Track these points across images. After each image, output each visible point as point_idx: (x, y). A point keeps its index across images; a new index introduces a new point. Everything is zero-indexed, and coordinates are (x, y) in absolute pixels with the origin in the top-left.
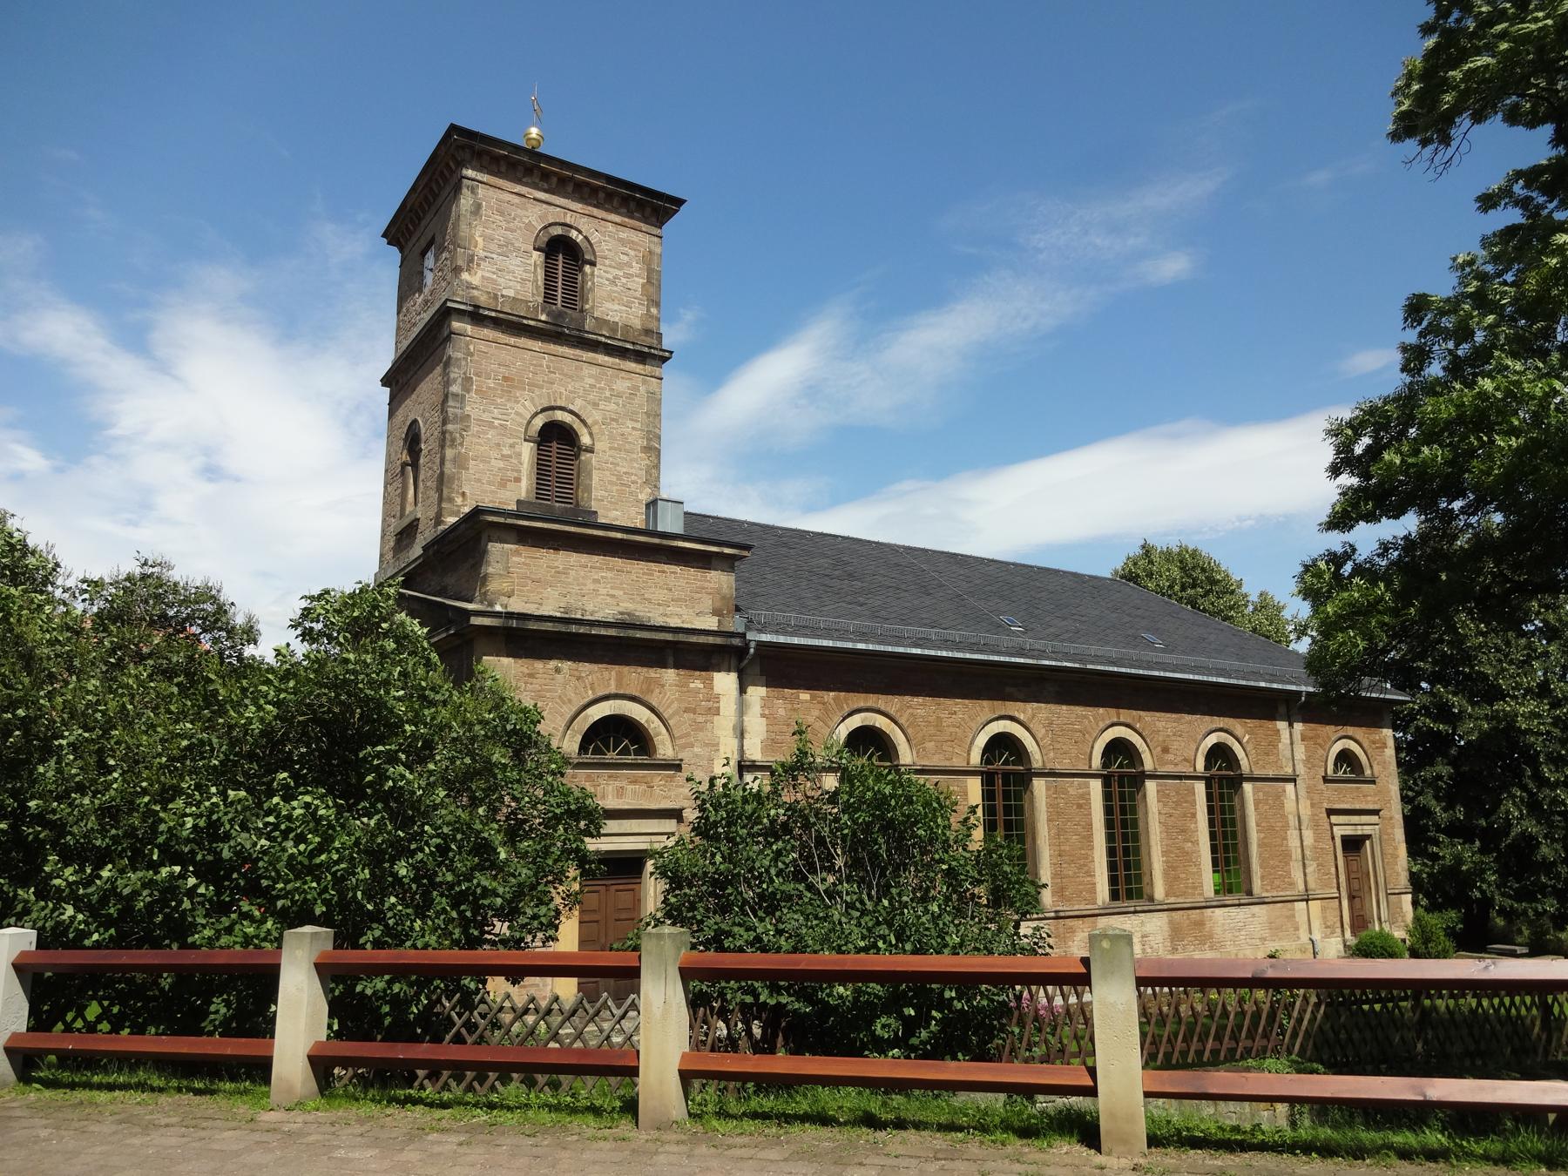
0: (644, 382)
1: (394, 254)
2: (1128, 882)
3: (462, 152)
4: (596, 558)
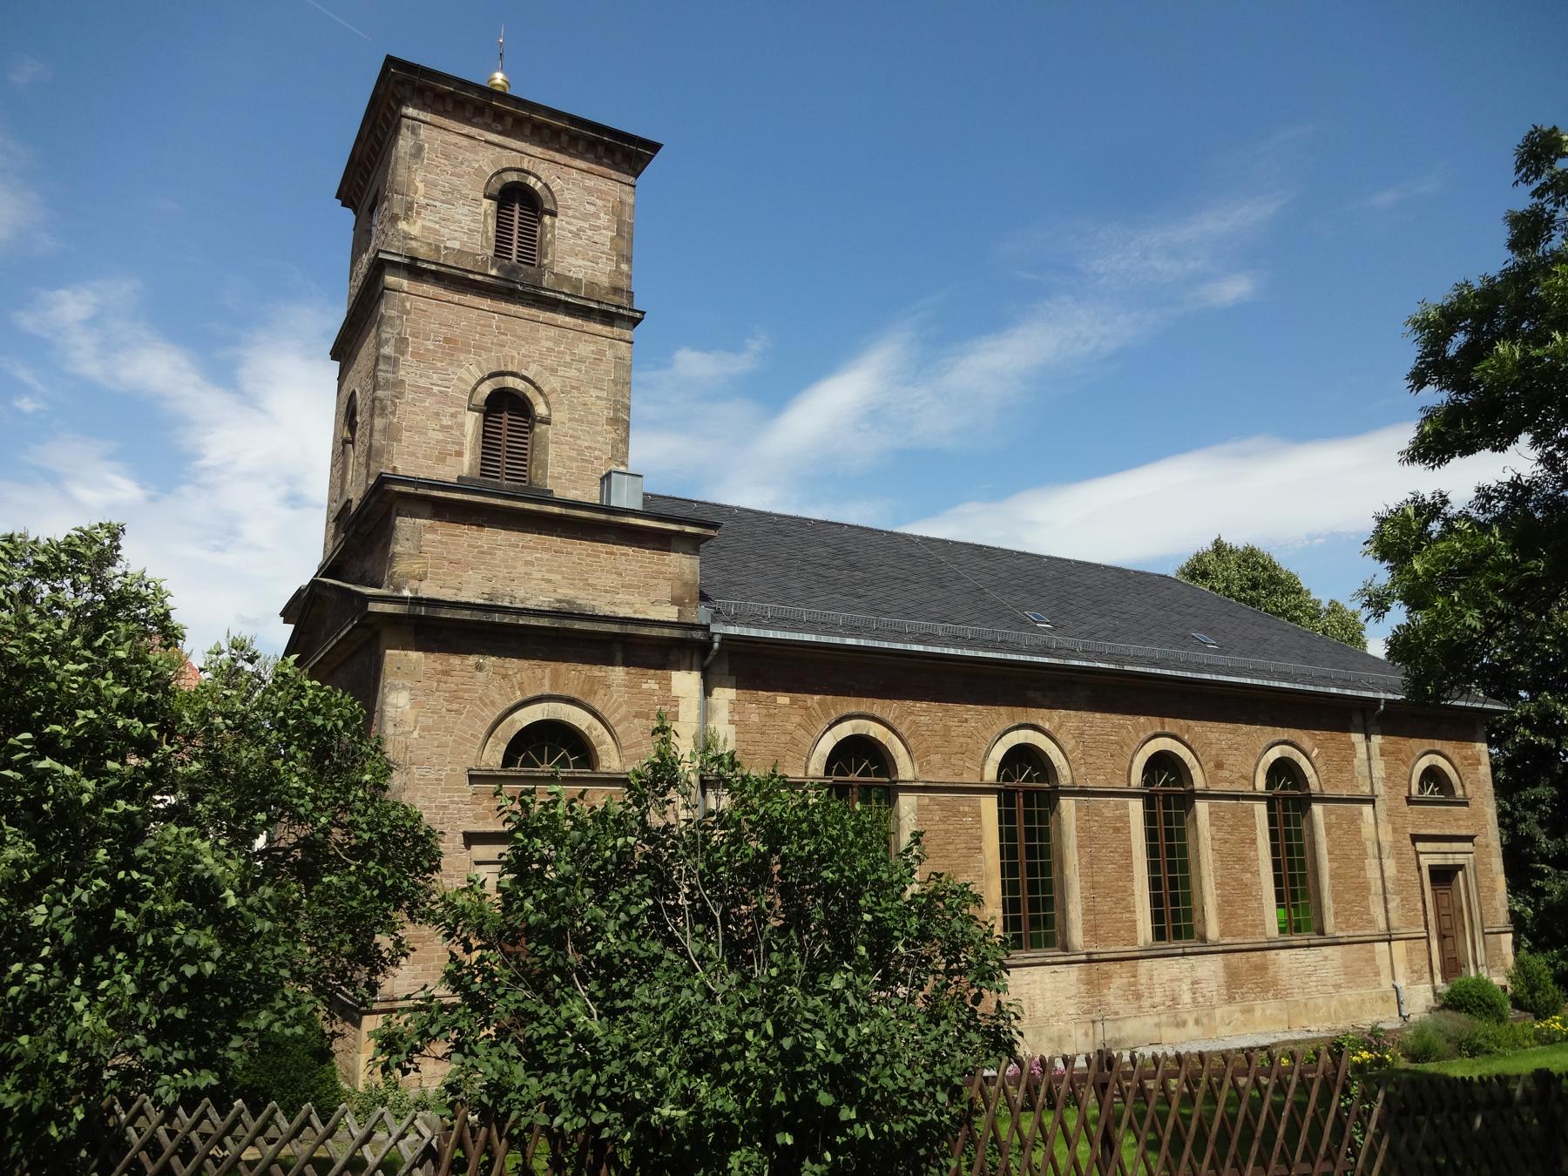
0: (611, 346)
1: (349, 216)
2: (1175, 918)
3: (404, 87)
4: (529, 536)
